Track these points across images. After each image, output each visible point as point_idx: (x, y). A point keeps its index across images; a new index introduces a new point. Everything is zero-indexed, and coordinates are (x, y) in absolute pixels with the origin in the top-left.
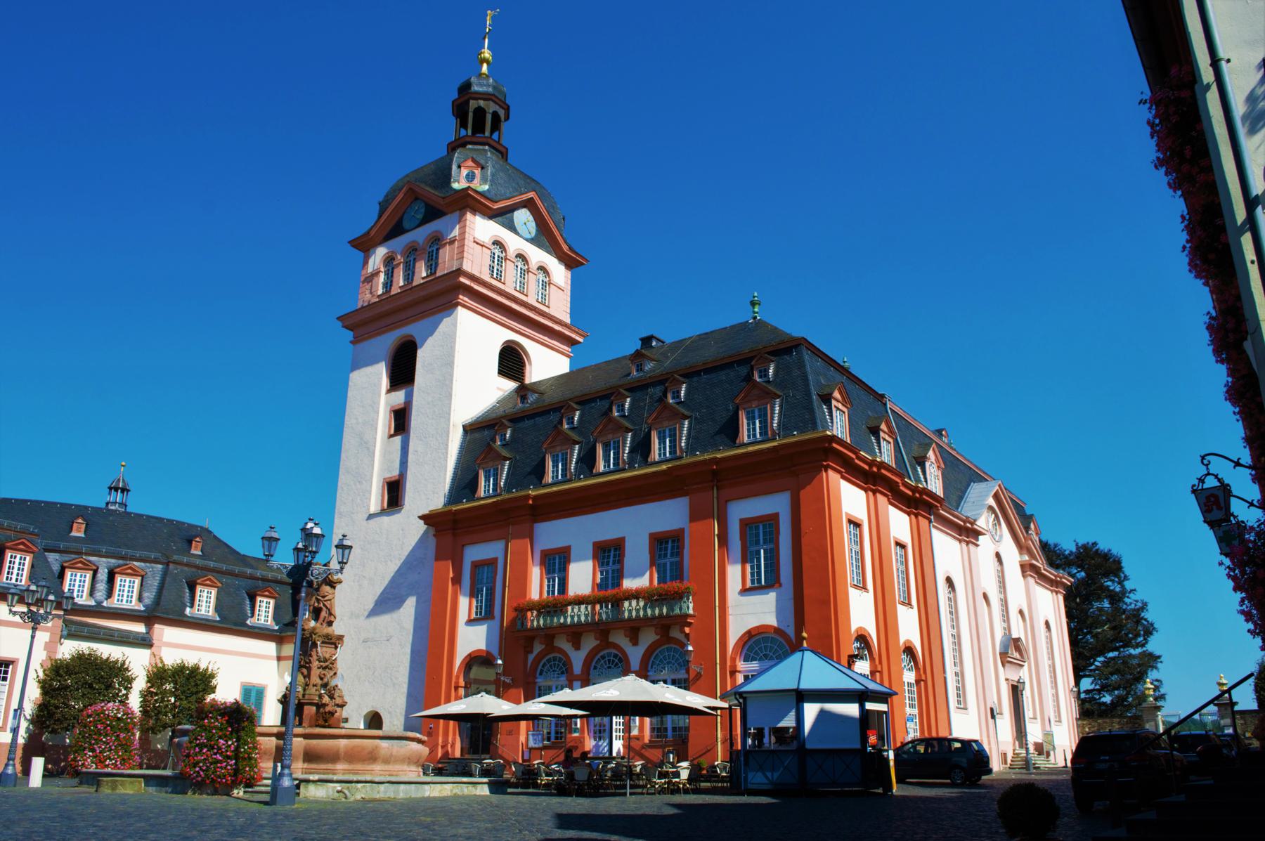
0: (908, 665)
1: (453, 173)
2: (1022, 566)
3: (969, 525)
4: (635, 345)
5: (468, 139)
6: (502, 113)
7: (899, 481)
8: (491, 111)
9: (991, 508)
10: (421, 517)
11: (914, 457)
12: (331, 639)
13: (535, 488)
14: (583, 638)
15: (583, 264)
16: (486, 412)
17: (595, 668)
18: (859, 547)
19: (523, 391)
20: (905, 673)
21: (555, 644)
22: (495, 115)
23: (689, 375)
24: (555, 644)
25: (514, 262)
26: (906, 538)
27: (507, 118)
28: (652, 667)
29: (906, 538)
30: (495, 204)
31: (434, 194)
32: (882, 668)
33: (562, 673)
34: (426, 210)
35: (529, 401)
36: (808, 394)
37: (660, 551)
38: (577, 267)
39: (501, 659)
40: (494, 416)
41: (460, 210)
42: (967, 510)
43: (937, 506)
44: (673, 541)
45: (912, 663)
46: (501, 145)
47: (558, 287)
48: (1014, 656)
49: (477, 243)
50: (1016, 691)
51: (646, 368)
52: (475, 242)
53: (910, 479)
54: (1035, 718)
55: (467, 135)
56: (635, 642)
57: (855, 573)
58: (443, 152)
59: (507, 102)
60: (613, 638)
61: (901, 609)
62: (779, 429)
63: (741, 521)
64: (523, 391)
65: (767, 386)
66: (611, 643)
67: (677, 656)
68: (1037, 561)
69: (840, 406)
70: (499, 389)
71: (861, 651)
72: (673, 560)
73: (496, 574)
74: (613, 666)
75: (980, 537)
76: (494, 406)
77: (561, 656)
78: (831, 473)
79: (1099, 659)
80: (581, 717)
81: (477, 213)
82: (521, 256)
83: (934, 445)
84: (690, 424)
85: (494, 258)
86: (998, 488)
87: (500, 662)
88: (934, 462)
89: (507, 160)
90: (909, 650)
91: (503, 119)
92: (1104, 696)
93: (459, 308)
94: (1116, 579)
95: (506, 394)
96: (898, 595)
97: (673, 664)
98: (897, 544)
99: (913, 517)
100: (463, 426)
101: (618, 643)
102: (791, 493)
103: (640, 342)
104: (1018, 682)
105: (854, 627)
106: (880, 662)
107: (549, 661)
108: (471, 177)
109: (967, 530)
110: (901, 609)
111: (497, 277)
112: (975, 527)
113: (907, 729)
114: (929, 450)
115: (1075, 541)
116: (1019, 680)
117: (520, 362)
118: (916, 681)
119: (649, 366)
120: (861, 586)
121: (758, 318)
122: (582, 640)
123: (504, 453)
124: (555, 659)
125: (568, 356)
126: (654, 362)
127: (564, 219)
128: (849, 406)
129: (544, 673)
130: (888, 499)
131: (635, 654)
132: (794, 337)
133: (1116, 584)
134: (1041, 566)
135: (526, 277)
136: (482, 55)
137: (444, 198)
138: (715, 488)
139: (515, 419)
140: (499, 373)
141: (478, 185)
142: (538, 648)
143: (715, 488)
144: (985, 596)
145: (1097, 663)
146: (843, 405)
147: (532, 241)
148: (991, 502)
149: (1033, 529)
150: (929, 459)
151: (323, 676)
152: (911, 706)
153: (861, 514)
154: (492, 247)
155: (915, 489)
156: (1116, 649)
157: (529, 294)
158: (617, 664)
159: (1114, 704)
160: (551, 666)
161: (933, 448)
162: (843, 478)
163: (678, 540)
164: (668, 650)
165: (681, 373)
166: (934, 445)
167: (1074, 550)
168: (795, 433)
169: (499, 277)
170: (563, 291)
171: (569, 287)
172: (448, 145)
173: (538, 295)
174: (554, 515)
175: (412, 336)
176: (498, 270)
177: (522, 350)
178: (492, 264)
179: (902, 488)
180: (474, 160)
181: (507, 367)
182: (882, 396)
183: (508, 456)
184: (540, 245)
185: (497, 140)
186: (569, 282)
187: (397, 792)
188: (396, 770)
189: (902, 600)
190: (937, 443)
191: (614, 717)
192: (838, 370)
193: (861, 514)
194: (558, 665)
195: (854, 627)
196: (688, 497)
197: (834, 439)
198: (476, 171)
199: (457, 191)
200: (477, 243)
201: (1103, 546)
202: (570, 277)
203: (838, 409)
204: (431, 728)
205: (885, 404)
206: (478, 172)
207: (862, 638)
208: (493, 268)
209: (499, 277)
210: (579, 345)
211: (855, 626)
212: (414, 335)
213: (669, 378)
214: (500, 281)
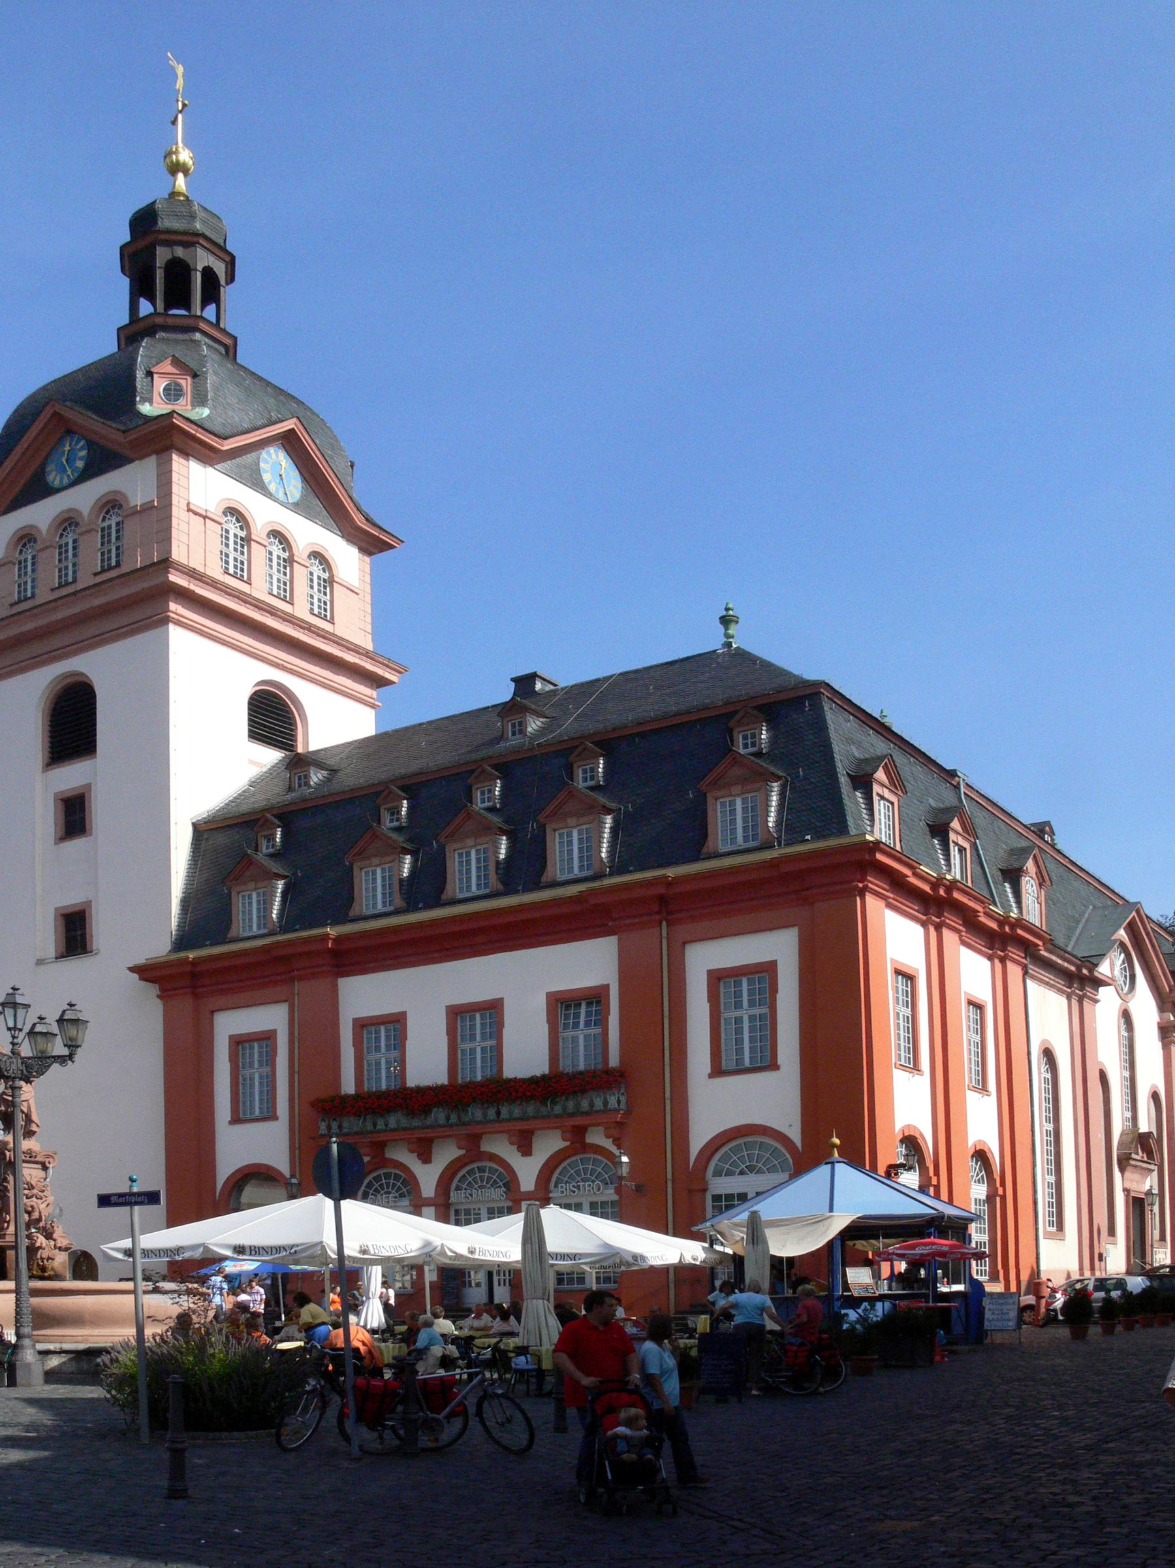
0: (978, 1175)
1: (138, 385)
4: (504, 693)
5: (159, 320)
6: (220, 269)
7: (977, 907)
8: (200, 268)
9: (1122, 945)
10: (132, 969)
11: (1000, 869)
12: (35, 1157)
13: (335, 923)
15: (395, 547)
16: (232, 801)
17: (458, 1188)
18: (910, 1010)
19: (298, 763)
20: (973, 1187)
21: (387, 1155)
22: (208, 273)
23: (607, 744)
24: (387, 1155)
25: (265, 546)
26: (984, 994)
27: (231, 278)
28: (556, 1186)
29: (984, 994)
30: (226, 442)
31: (109, 432)
33: (402, 1196)
34: (88, 453)
35: (312, 783)
36: (833, 775)
37: (567, 1017)
38: (382, 551)
39: (625, 1154)
40: (244, 808)
41: (158, 452)
44: (589, 1004)
45: (983, 1172)
46: (224, 331)
47: (348, 588)
49: (196, 513)
51: (529, 729)
52: (189, 510)
53: (996, 905)
55: (156, 314)
56: (526, 1150)
57: (902, 1048)
58: (109, 346)
59: (229, 248)
60: (488, 1146)
61: (972, 1098)
62: (779, 831)
64: (298, 763)
65: (758, 761)
66: (484, 1152)
67: (399, 1184)
69: (887, 794)
70: (251, 762)
72: (588, 1032)
75: (1101, 989)
76: (244, 792)
77: (397, 1172)
78: (870, 899)
81: (191, 458)
82: (278, 535)
83: (1036, 851)
84: (615, 820)
85: (227, 538)
86: (1134, 913)
87: (625, 1159)
90: (981, 1156)
91: (223, 281)
93: (171, 626)
95: (264, 770)
97: (593, 1182)
99: (997, 961)
100: (194, 824)
101: (496, 1153)
102: (799, 929)
103: (513, 685)
105: (899, 1125)
106: (937, 1173)
107: (377, 1179)
108: (173, 392)
110: (972, 1098)
111: (320, 613)
119: (533, 725)
120: (912, 1066)
121: (734, 646)
122: (534, 1145)
123: (275, 867)
124: (387, 1176)
125: (373, 706)
126: (544, 720)
127: (352, 466)
128: (900, 793)
130: (960, 937)
131: (428, 1177)
132: (808, 681)
135: (245, 550)
136: (174, 157)
137: (124, 432)
138: (664, 923)
139: (286, 816)
140: (250, 736)
141: (189, 407)
143: (664, 923)
146: (964, 838)
147: (298, 507)
148: (1122, 934)
150: (1027, 872)
151: (30, 1209)
154: (223, 520)
155: (1003, 921)
160: (750, 1157)
161: (1034, 856)
162: (890, 906)
163: (598, 1002)
164: (481, 1170)
165: (597, 739)
166: (1036, 851)
168: (808, 837)
169: (239, 571)
170: (357, 594)
171: (368, 589)
172: (119, 330)
173: (271, 583)
174: (389, 962)
175: (82, 674)
176: (236, 560)
177: (289, 699)
178: (225, 550)
180: (176, 362)
182: (952, 774)
183: (282, 872)
184: (310, 515)
185: (214, 320)
186: (368, 579)
189: (974, 1084)
190: (1039, 847)
192: (882, 735)
195: (899, 1125)
196: (616, 937)
197: (877, 845)
198: (183, 382)
199: (148, 420)
200: (196, 513)
202: (368, 570)
203: (882, 798)
205: (957, 787)
206: (186, 383)
207: (911, 1142)
208: (227, 555)
209: (239, 571)
210: (394, 685)
212: (84, 671)
213: (577, 746)
214: (241, 579)
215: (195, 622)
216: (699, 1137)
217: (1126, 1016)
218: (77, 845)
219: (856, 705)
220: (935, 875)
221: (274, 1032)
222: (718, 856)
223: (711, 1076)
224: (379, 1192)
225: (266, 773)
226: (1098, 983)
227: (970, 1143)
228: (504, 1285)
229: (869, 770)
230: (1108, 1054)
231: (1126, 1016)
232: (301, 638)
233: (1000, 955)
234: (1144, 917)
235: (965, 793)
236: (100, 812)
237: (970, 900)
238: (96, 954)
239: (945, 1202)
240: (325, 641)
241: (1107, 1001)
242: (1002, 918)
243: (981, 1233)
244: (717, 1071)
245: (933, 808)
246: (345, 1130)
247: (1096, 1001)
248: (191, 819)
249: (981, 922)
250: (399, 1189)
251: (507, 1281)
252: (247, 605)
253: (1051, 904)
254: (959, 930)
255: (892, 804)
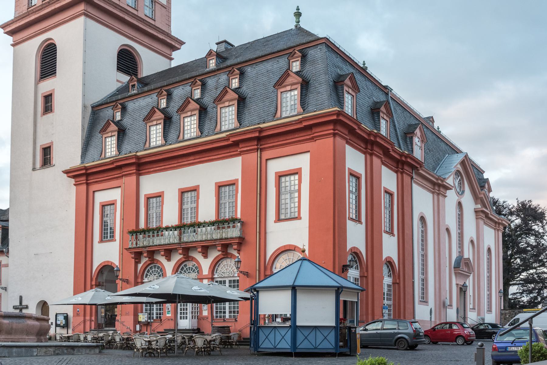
2: (476, 212)
3: (440, 182)
14: (172, 253)
28: (216, 273)
32: (368, 274)
42: (440, 172)
43: (417, 168)
45: (391, 272)
48: (464, 270)
50: (463, 290)
54: (474, 309)
61: (385, 237)
63: (276, 173)
68: (487, 208)
70: (118, 81)
71: (352, 262)
73: (116, 211)
74: (192, 272)
79: (523, 274)
80: (156, 303)
88: (420, 137)
89: (462, 152)
92: (523, 297)
94: (540, 224)
96: (385, 224)
98: (386, 192)
104: (463, 286)
106: (367, 271)
109: (439, 185)
110: (385, 236)
112: (445, 183)
113: (383, 314)
114: (416, 128)
115: (517, 199)
116: (464, 284)
117: (134, 64)
118: (360, 276)
120: (357, 220)
129: (148, 276)
130: (382, 161)
133: (540, 227)
134: (489, 213)
140: (118, 69)
142: (144, 260)
144: (448, 230)
145: (521, 277)
146: (353, 90)
149: (487, 188)
152: (388, 299)
153: (360, 169)
156: (535, 268)
157: (139, 9)
158: (194, 270)
159: (529, 302)
167: (516, 205)
170: (166, 8)
179: (392, 153)
181: (126, 66)
187: (94, 351)
188: (17, 338)
191: (179, 304)
193: (360, 169)
194: (157, 271)
201: (534, 204)
204: (78, 311)
207: (356, 253)
211: (386, 254)
215: (102, 19)
216: (271, 249)
217: (460, 204)
218: (50, 115)
219: (342, 51)
220: (369, 130)
221: (238, 179)
222: (281, 118)
223: (275, 222)
224: (186, 272)
225: (125, 86)
226: (447, 188)
227: (384, 257)
228: (195, 318)
229: (342, 79)
230: (450, 220)
231: (460, 204)
232: (140, 26)
233: (401, 171)
234: (468, 159)
235: (391, 97)
236: (57, 102)
237: (385, 143)
238: (54, 165)
239: (332, 272)
240: (150, 28)
241: (451, 197)
242: (401, 153)
243: (389, 301)
244: (278, 219)
245: (374, 101)
246: (138, 246)
247: (446, 196)
248: (91, 105)
249: (391, 154)
250: (159, 273)
251: (196, 317)
252: (117, 9)
253: (427, 151)
254: (381, 157)
255: (353, 96)
